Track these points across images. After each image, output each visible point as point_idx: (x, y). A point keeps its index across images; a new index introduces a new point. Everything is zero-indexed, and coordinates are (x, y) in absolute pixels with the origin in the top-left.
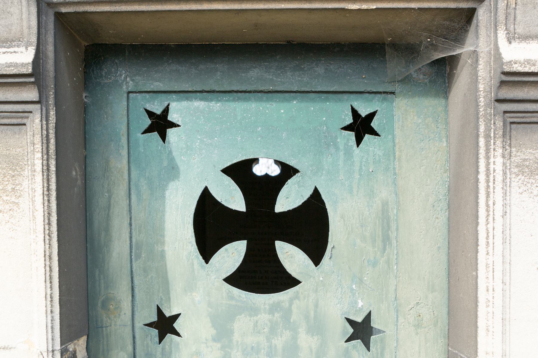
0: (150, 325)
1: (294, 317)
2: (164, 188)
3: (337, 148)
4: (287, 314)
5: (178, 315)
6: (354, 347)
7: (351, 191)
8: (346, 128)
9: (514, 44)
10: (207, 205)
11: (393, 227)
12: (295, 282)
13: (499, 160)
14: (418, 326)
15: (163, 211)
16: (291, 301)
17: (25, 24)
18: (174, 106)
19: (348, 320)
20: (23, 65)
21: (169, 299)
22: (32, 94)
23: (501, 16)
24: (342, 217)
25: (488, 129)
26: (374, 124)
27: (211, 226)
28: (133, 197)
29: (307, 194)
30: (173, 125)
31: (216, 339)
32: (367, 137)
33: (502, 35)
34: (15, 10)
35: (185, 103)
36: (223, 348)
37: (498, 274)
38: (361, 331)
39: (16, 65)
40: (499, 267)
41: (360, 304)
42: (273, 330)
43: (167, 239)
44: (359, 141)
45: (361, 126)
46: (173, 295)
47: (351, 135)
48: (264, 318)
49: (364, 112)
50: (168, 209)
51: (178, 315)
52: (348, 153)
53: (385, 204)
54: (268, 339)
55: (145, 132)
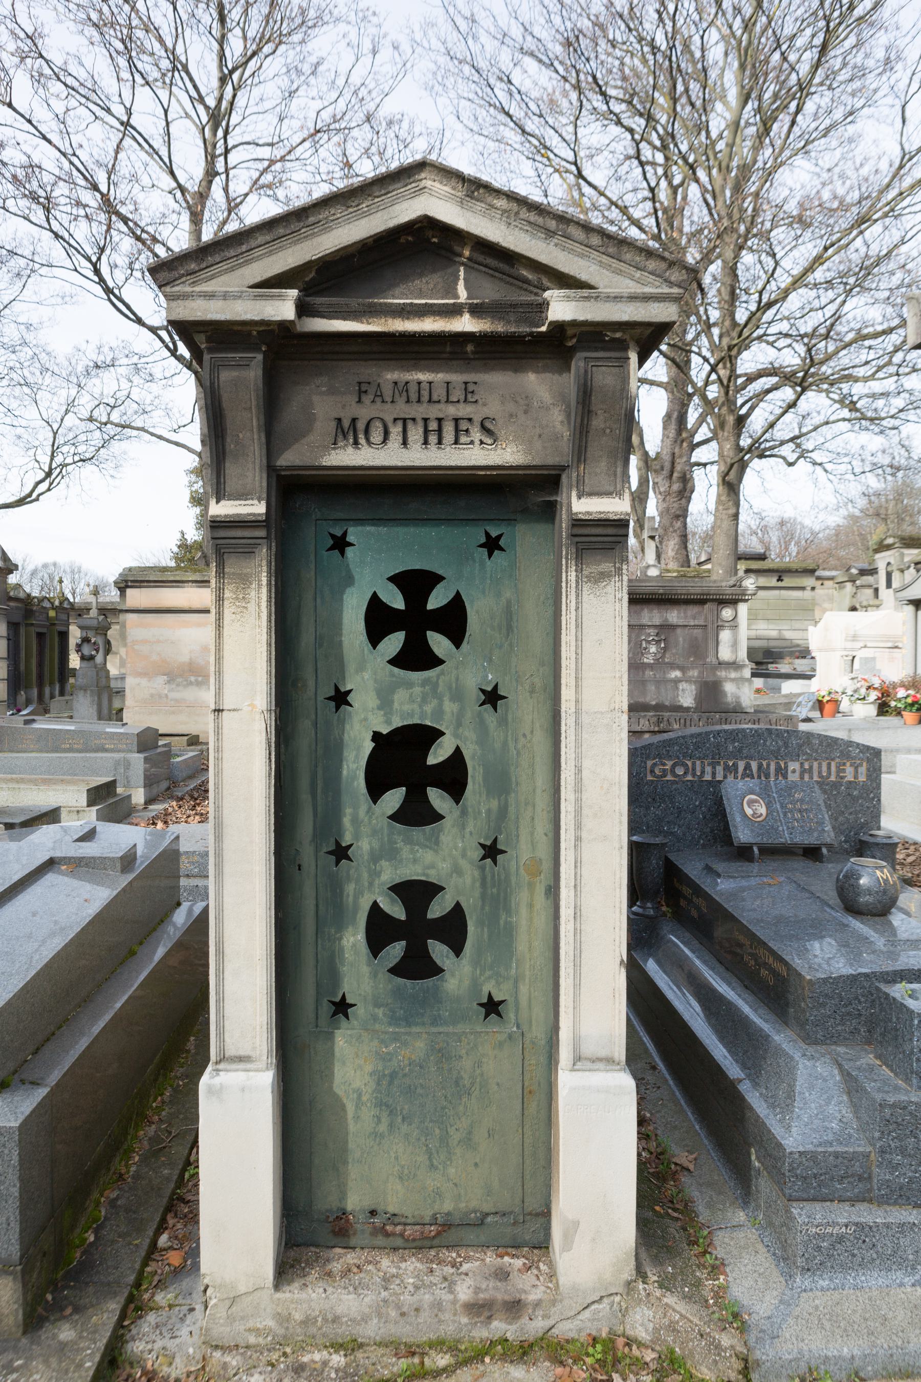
0: (329, 699)
1: (440, 689)
2: (342, 593)
3: (474, 561)
4: (435, 686)
5: (350, 691)
6: (485, 710)
7: (484, 593)
8: (481, 546)
9: (583, 500)
10: (375, 604)
11: (515, 618)
12: (440, 662)
13: (574, 574)
14: (532, 692)
15: (342, 611)
16: (438, 677)
17: (257, 483)
18: (351, 530)
19: (482, 690)
20: (259, 515)
21: (344, 678)
22: (262, 533)
23: (574, 483)
24: (477, 612)
25: (567, 554)
26: (502, 543)
27: (379, 620)
28: (318, 600)
29: (451, 595)
30: (351, 545)
31: (380, 708)
32: (496, 552)
33: (574, 494)
34: (250, 474)
35: (360, 528)
36: (385, 715)
37: (573, 648)
38: (492, 697)
39: (254, 515)
40: (573, 643)
41: (490, 677)
42: (424, 700)
43: (344, 632)
44: (490, 555)
45: (492, 545)
46: (347, 675)
47: (485, 551)
48: (417, 690)
49: (494, 534)
50: (345, 608)
51: (350, 691)
52: (482, 564)
53: (509, 602)
54: (421, 707)
55: (328, 550)
